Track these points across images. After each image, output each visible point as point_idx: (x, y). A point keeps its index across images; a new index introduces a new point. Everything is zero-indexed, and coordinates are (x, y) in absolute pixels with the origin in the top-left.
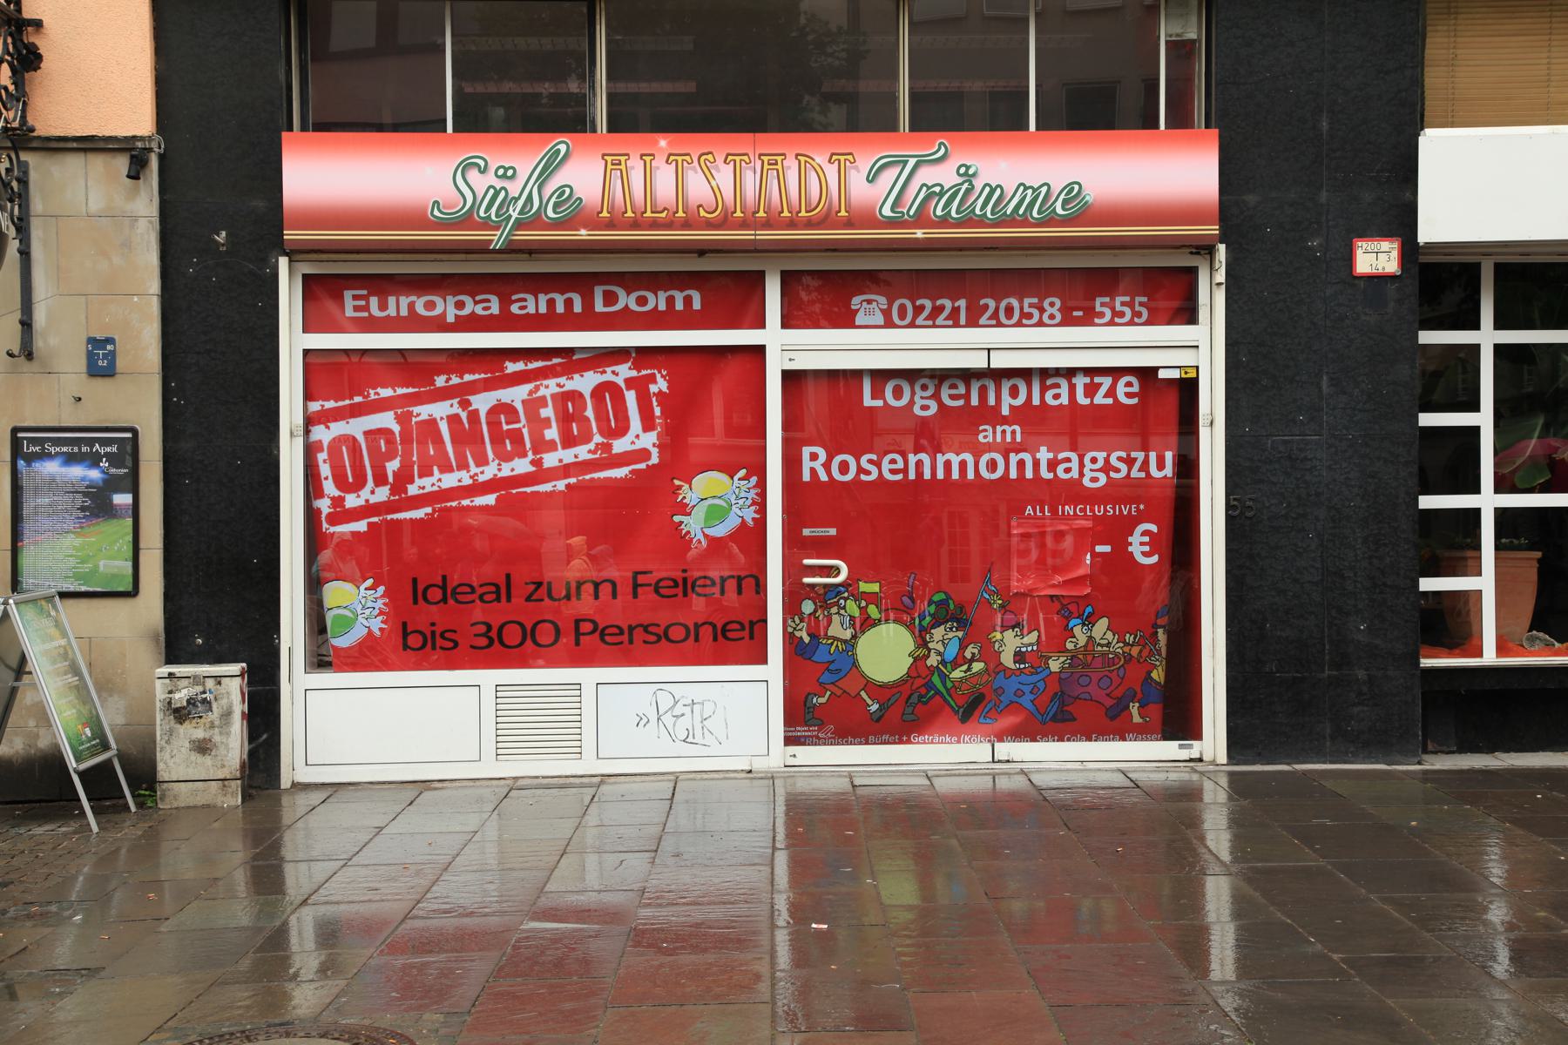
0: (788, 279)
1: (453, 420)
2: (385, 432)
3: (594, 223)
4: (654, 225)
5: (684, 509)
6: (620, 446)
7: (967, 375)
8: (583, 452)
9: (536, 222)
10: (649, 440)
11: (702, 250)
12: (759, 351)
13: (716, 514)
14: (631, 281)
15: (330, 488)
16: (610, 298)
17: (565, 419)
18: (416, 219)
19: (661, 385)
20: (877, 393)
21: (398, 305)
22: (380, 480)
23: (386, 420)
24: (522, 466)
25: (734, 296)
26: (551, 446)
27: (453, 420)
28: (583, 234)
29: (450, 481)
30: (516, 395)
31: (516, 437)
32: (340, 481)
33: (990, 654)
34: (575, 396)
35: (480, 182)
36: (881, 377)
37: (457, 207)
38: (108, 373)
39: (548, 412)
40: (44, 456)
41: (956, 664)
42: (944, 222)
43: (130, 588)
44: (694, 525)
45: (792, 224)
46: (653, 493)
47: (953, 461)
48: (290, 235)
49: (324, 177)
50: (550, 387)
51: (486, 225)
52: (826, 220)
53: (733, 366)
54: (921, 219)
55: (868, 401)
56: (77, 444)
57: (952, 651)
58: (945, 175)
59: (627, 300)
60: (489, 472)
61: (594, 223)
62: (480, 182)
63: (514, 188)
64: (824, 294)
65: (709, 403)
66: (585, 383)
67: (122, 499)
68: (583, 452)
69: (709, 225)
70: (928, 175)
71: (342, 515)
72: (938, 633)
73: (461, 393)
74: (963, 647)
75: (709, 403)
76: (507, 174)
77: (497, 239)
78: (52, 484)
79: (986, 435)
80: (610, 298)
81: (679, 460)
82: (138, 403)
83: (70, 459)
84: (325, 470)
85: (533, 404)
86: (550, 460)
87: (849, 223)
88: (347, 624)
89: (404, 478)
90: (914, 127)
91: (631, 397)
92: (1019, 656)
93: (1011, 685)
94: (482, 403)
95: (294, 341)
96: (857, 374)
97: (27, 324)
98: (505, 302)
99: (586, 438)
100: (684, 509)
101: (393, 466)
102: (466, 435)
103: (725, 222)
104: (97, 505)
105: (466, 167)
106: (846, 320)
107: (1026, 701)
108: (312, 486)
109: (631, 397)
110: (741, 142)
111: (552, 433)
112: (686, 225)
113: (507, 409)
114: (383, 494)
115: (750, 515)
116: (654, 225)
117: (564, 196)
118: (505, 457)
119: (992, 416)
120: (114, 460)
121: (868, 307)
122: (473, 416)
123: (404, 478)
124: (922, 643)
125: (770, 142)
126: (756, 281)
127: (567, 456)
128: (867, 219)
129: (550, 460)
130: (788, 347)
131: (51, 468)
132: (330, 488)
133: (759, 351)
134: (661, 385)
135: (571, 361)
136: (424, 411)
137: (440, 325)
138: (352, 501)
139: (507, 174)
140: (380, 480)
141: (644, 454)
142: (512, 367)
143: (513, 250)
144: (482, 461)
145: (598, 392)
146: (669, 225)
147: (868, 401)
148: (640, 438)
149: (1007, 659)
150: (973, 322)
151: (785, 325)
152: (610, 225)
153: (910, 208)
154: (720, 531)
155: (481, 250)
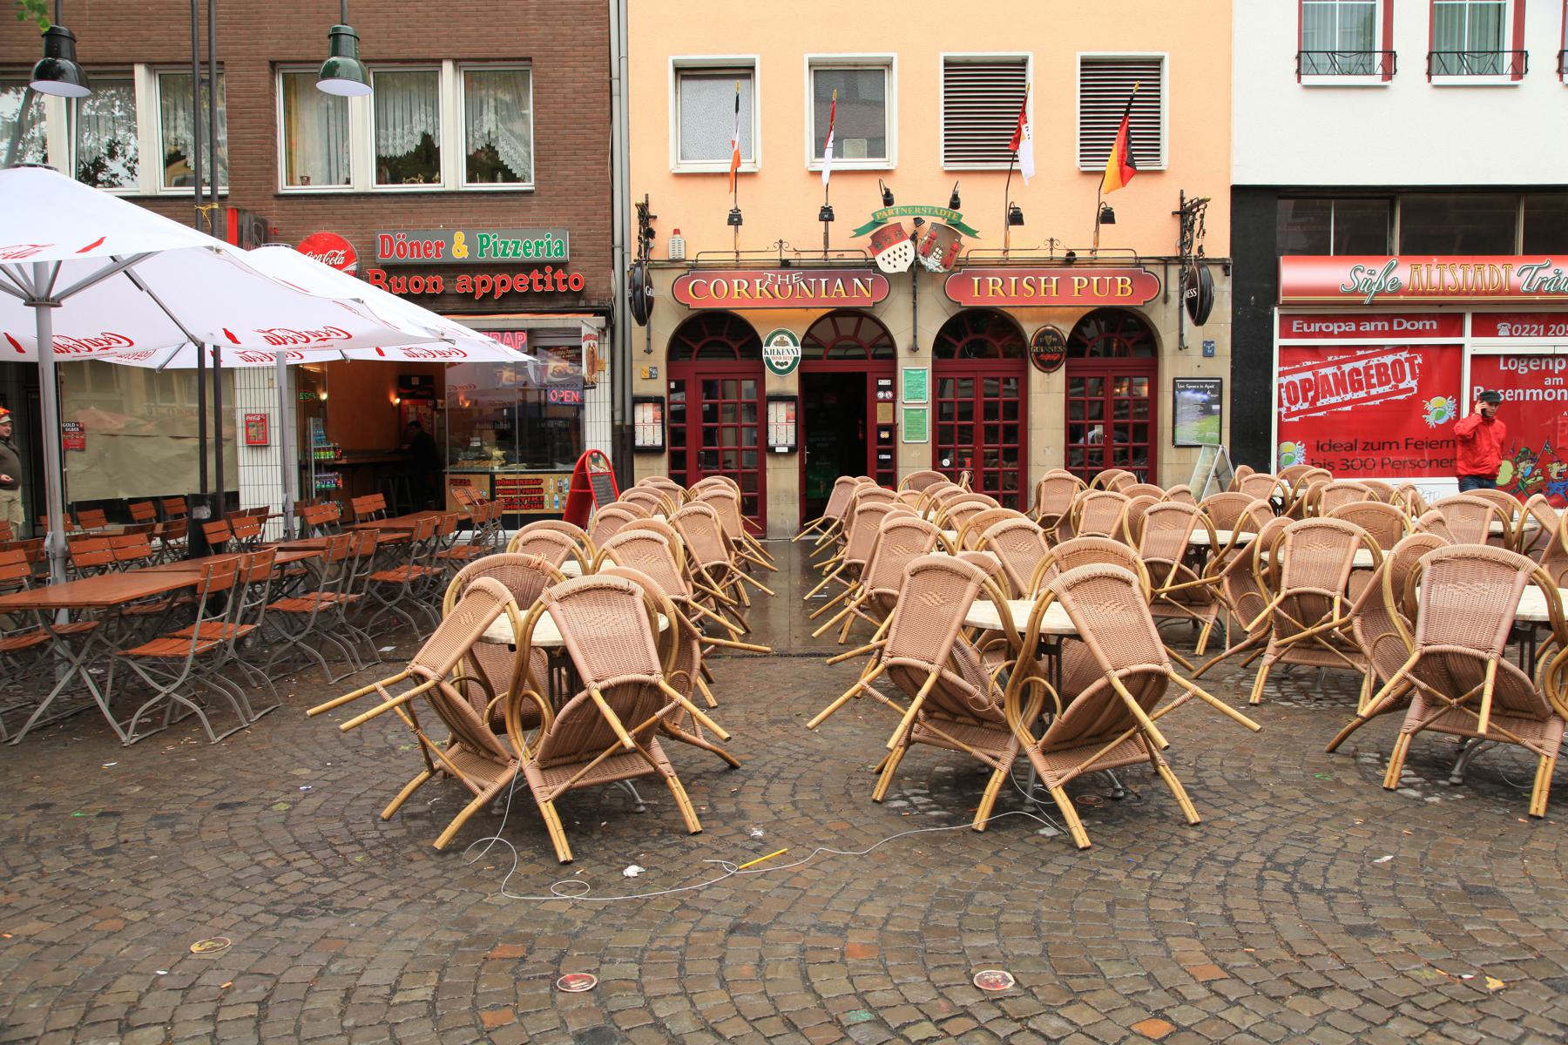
0: (1474, 316)
1: (1335, 375)
2: (1308, 380)
3: (1406, 293)
4: (1431, 294)
5: (1427, 412)
6: (1402, 386)
7: (1541, 357)
8: (1386, 389)
9: (1383, 293)
10: (1414, 384)
11: (1440, 304)
12: (1461, 346)
13: (1440, 415)
14: (1409, 317)
15: (1286, 403)
16: (1400, 324)
17: (1379, 374)
18: (1335, 292)
19: (1419, 361)
20: (1506, 364)
21: (1315, 327)
22: (1305, 400)
23: (1309, 375)
24: (1362, 394)
25: (1451, 323)
26: (1374, 386)
27: (1335, 375)
28: (1402, 298)
29: (1333, 400)
30: (1360, 365)
31: (1360, 382)
32: (1289, 399)
33: (1545, 473)
34: (1385, 365)
35: (1361, 276)
36: (1507, 357)
37: (1352, 287)
38: (1211, 355)
39: (1373, 372)
40: (1185, 389)
41: (1529, 477)
42: (1548, 293)
43: (1179, 442)
44: (1431, 420)
45: (1486, 294)
46: (1414, 406)
47: (1535, 394)
48: (1282, 298)
49: (1297, 274)
50: (1374, 361)
51: (1363, 294)
52: (1500, 292)
53: (1449, 353)
54: (1539, 292)
55: (1502, 368)
56: (1198, 384)
57: (1528, 472)
58: (1549, 274)
59: (1407, 325)
60: (1348, 397)
61: (1406, 293)
62: (1361, 276)
63: (1375, 279)
64: (1486, 324)
65: (1441, 371)
66: (1388, 359)
67: (1216, 407)
68: (1386, 389)
69: (1453, 294)
70: (1542, 274)
71: (1290, 414)
72: (1522, 464)
73: (1338, 364)
74: (1533, 469)
75: (1441, 371)
76: (1372, 273)
77: (1367, 300)
78: (1188, 401)
79: (1548, 382)
80: (1400, 324)
81: (1425, 391)
82: (1222, 367)
83: (1197, 391)
84: (1284, 396)
85: (1368, 368)
86: (1373, 392)
87: (1509, 293)
88: (1290, 460)
89: (1315, 398)
90: (1403, 252)
91: (1407, 366)
92: (1559, 474)
93: (1556, 485)
94: (1347, 368)
95: (1278, 342)
96: (1498, 356)
97: (1181, 336)
98: (1358, 326)
99: (1388, 382)
100: (1427, 412)
101: (1311, 394)
102: (1340, 383)
103: (1459, 293)
104: (1206, 410)
105: (1356, 270)
106: (1495, 334)
107: (1561, 493)
108: (1280, 404)
109: (1407, 366)
110: (1467, 259)
111: (1374, 381)
112: (1444, 294)
113: (1357, 371)
114: (1306, 406)
115: (1452, 415)
116: (1431, 294)
117: (1395, 282)
118: (1355, 390)
119: (1552, 374)
120: (1213, 391)
121: (1503, 328)
122: (1343, 373)
123: (1315, 398)
124: (1516, 469)
125: (1478, 259)
126: (1461, 317)
127: (1381, 390)
128: (1516, 291)
129: (1373, 392)
130: (1473, 344)
131: (1188, 394)
132: (1286, 403)
133: (1461, 346)
134: (1419, 361)
135: (1383, 350)
136: (1323, 371)
137: (1383, 334)
138: (1294, 409)
139: (1372, 273)
140: (1305, 400)
141: (1411, 389)
142: (1359, 353)
143: (1373, 304)
144: (1346, 392)
145: (1394, 363)
146: (1436, 294)
147: (1502, 368)
148: (1410, 383)
149: (1554, 475)
150: (1545, 335)
151: (1474, 335)
152: (1413, 294)
153: (1534, 287)
154: (1441, 422)
155: (1360, 304)
